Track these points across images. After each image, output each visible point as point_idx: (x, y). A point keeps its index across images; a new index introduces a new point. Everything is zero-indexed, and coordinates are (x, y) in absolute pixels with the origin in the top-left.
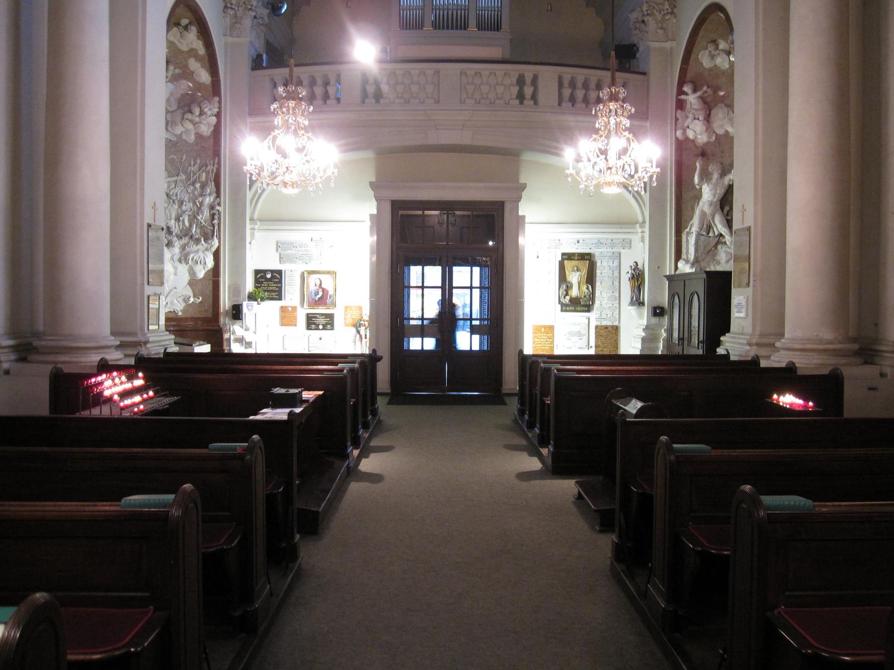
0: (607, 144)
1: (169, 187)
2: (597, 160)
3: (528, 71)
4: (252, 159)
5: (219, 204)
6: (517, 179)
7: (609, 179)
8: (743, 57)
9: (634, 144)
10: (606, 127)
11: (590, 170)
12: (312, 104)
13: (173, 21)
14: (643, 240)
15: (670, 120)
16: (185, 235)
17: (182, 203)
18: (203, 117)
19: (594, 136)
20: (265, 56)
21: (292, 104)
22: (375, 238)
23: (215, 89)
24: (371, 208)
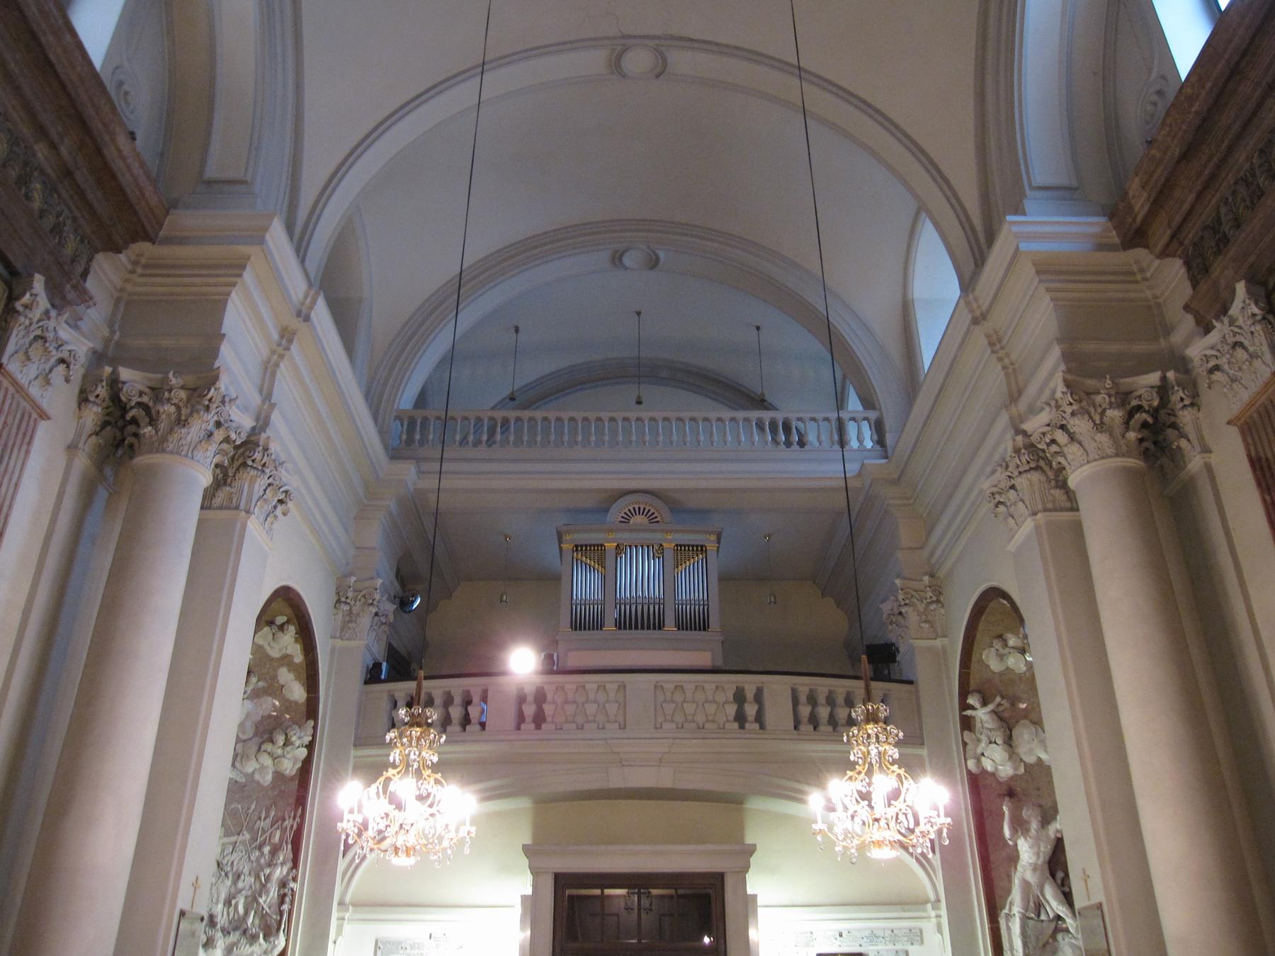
0: (869, 784)
1: (223, 851)
2: (857, 808)
3: (750, 683)
4: (351, 812)
5: (295, 879)
6: (740, 838)
7: (877, 836)
8: (1044, 655)
9: (909, 783)
10: (864, 759)
11: (848, 824)
12: (444, 731)
13: (265, 619)
14: (940, 930)
15: (955, 748)
16: (235, 929)
17: (239, 877)
18: (288, 748)
19: (849, 773)
20: (384, 666)
21: (416, 732)
22: (529, 933)
23: (311, 709)
24: (523, 884)
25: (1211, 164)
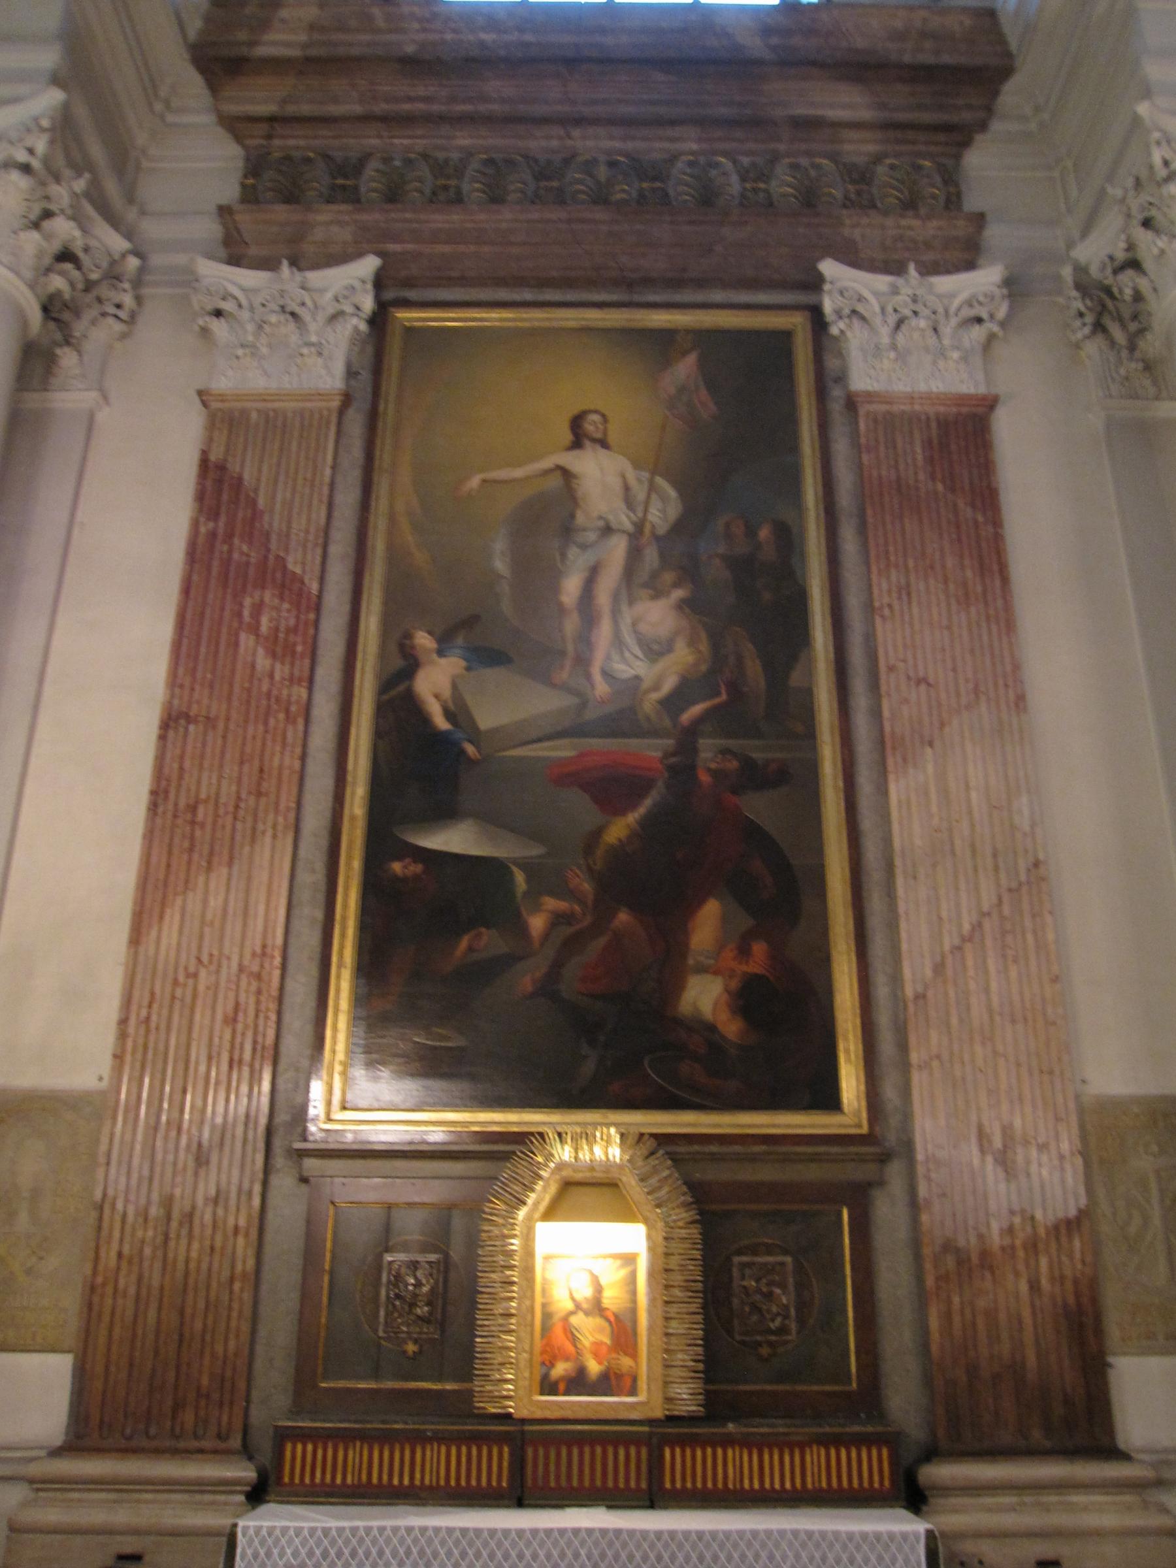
25: (421, 106)
